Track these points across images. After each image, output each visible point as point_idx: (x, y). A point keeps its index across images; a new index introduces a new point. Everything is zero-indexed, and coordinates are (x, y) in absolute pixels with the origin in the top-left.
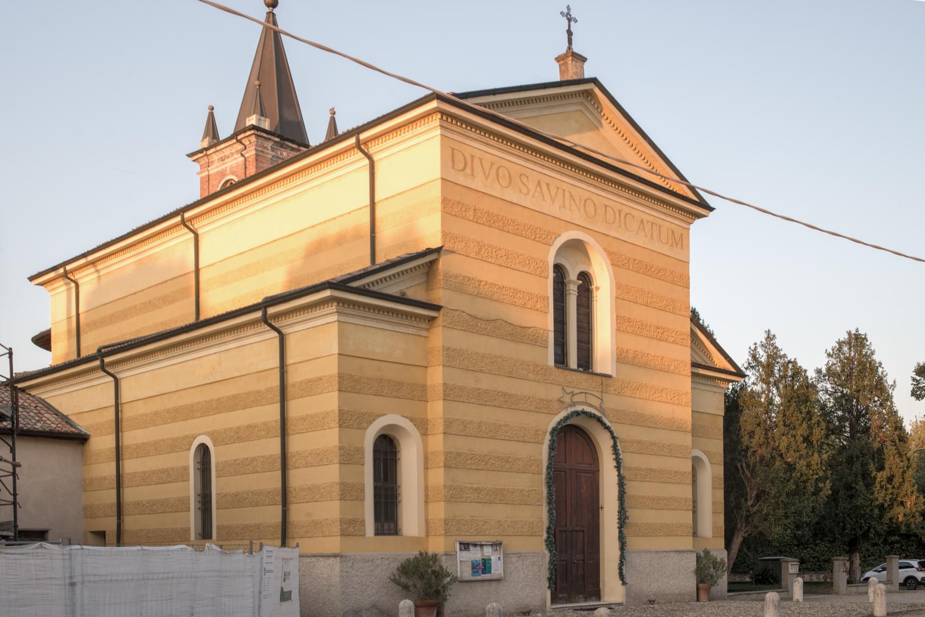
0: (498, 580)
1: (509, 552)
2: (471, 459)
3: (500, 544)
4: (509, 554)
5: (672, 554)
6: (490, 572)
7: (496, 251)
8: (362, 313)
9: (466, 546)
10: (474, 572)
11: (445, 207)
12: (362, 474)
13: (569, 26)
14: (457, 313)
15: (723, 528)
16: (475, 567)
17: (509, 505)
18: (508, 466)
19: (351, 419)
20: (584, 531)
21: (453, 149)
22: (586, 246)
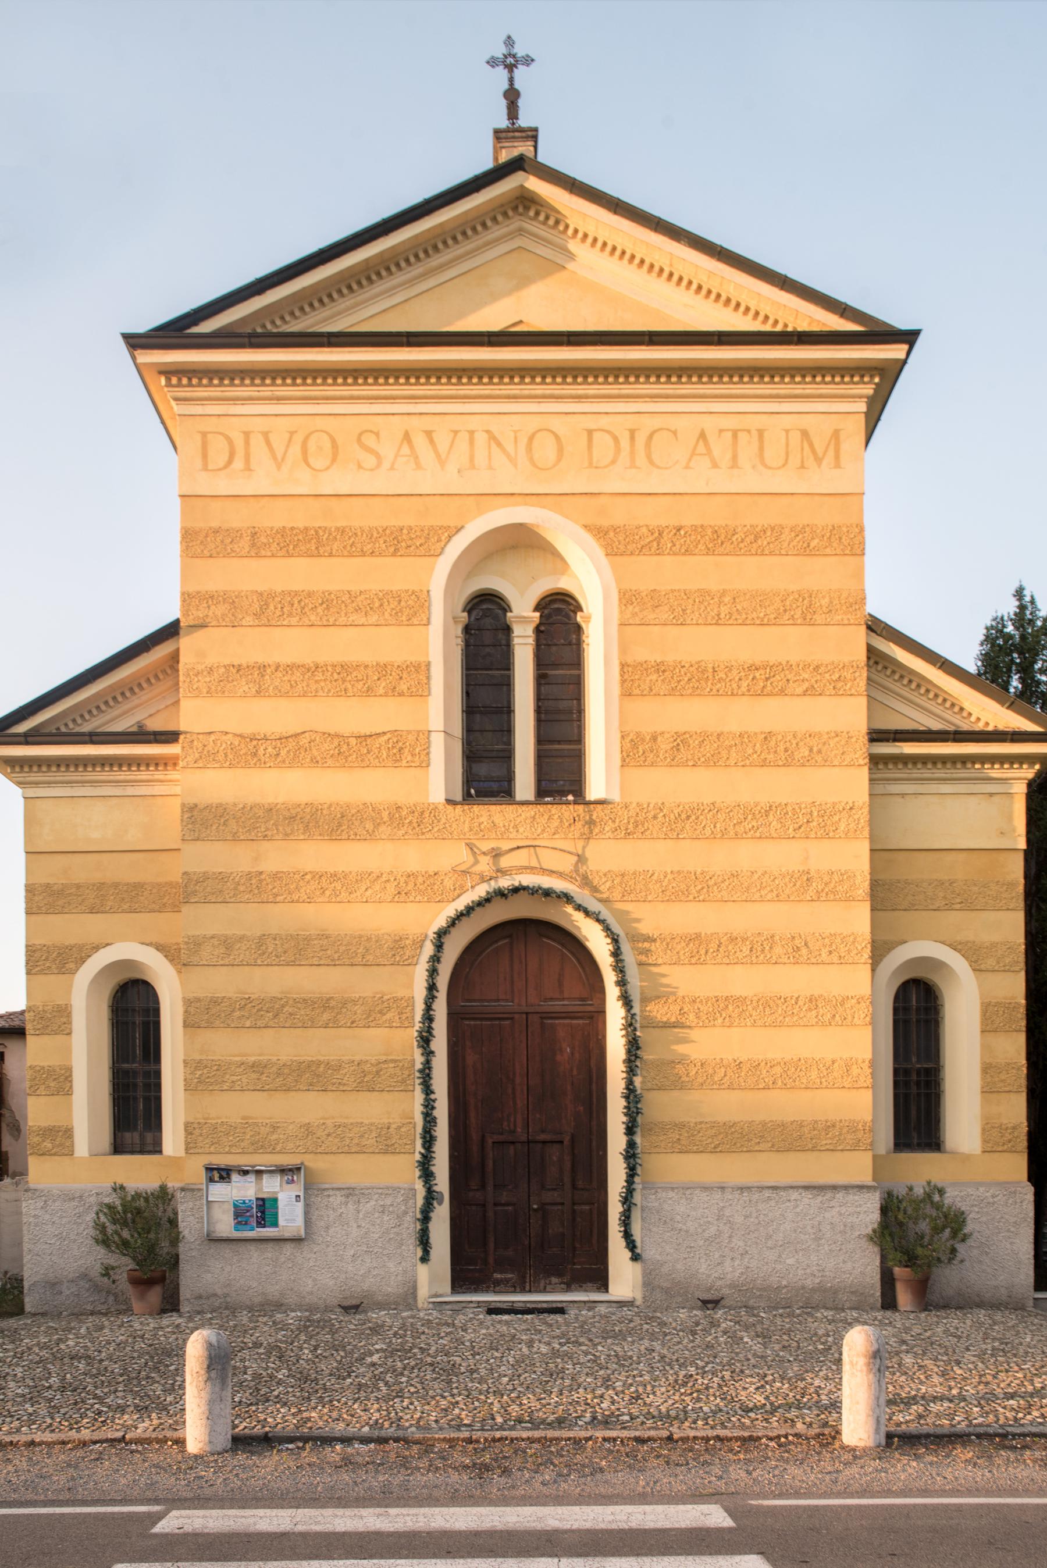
0: (297, 1240)
1: (327, 1186)
2: (242, 1008)
3: (299, 1169)
4: (324, 1190)
5: (794, 1195)
6: (275, 1224)
7: (299, 602)
8: (60, 776)
9: (224, 1174)
10: (239, 1223)
11: (187, 547)
12: (68, 1050)
13: (511, 80)
14: (213, 737)
15: (1024, 1128)
16: (240, 1213)
17: (330, 1093)
18: (326, 1016)
19: (47, 959)
20: (562, 1142)
21: (204, 434)
22: (536, 530)
